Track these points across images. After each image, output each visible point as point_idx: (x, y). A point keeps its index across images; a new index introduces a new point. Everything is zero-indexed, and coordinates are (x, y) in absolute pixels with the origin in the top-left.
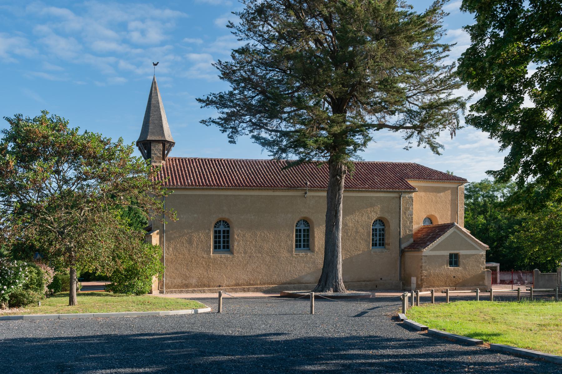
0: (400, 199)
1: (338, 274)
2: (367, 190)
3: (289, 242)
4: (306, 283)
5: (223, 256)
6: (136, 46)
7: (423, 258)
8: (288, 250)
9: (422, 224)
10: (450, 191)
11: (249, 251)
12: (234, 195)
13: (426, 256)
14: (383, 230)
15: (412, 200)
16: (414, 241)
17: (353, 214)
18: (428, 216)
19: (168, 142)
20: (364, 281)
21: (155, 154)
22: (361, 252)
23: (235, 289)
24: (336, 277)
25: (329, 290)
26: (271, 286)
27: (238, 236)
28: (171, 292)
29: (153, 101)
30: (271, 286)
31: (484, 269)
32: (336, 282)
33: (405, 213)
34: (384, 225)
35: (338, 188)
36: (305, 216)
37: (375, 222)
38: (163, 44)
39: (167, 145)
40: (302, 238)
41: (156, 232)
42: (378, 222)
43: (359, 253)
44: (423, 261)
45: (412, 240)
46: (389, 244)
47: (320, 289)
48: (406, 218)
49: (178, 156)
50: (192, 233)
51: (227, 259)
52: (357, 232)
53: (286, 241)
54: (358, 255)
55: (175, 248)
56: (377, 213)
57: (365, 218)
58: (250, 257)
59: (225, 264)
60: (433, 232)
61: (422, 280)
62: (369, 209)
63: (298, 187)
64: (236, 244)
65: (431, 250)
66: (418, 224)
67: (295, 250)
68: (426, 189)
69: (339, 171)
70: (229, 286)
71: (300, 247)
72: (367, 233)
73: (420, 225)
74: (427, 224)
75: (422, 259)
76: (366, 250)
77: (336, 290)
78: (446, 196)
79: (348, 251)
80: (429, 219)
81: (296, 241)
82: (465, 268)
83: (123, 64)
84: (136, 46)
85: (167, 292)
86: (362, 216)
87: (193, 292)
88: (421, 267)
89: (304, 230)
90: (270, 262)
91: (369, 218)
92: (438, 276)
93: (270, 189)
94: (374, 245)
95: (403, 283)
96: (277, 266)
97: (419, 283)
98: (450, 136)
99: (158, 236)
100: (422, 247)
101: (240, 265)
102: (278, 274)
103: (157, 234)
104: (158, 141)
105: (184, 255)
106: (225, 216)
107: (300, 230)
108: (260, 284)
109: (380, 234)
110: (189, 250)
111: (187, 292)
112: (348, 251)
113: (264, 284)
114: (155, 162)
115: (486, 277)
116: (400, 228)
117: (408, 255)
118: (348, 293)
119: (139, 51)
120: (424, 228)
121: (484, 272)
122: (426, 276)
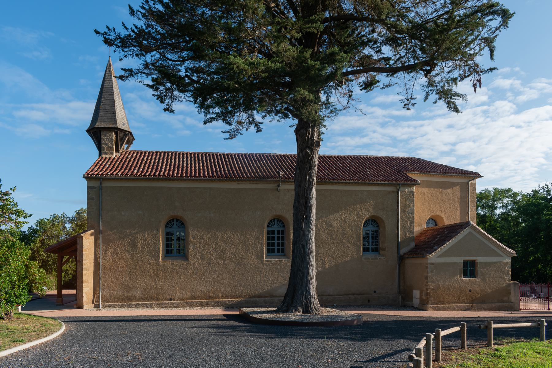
0: (398, 194)
1: (309, 287)
2: (356, 181)
3: (259, 246)
5: (175, 262)
7: (429, 266)
8: (257, 256)
9: (425, 226)
10: (458, 187)
11: (208, 256)
12: (189, 188)
13: (433, 264)
14: (377, 232)
15: (413, 195)
16: (416, 246)
17: (338, 212)
18: (432, 216)
19: (122, 130)
20: (353, 294)
21: (106, 144)
22: (349, 259)
23: (190, 303)
24: (307, 291)
25: (296, 310)
26: (236, 300)
27: (194, 238)
28: (110, 307)
29: (106, 85)
30: (236, 300)
31: (509, 281)
32: (306, 298)
34: (378, 226)
35: (308, 166)
36: (278, 214)
37: (366, 222)
39: (124, 136)
41: (89, 232)
42: (370, 222)
43: (347, 259)
44: (429, 270)
45: (413, 245)
46: (384, 249)
47: (285, 308)
48: (406, 216)
49: (137, 149)
50: (136, 233)
51: (180, 266)
53: (255, 245)
54: (346, 262)
56: (368, 211)
58: (209, 264)
59: (177, 272)
60: (440, 234)
61: (427, 294)
62: (359, 206)
63: (269, 178)
64: (191, 247)
65: (441, 256)
66: (420, 225)
67: (267, 256)
68: (429, 185)
69: (310, 142)
70: (182, 300)
71: (273, 252)
73: (423, 227)
74: (431, 225)
75: (427, 268)
76: (355, 256)
77: (306, 310)
78: (454, 193)
79: (333, 257)
80: (434, 220)
81: (268, 245)
82: (484, 280)
85: (104, 307)
86: (350, 214)
87: (137, 306)
88: (427, 278)
89: (278, 231)
90: (234, 270)
91: (358, 217)
92: (448, 289)
93: (234, 180)
94: (366, 250)
95: (402, 297)
97: (424, 298)
98: (473, 89)
99: (93, 237)
100: (427, 252)
101: (196, 274)
103: (91, 235)
104: (109, 129)
106: (179, 213)
107: (273, 231)
108: (223, 297)
109: (374, 236)
110: (133, 256)
111: (130, 306)
112: (333, 257)
113: (227, 297)
114: (106, 153)
115: (512, 291)
116: (398, 229)
117: (410, 262)
118: (326, 312)
120: (427, 230)
121: (509, 285)
122: (433, 289)
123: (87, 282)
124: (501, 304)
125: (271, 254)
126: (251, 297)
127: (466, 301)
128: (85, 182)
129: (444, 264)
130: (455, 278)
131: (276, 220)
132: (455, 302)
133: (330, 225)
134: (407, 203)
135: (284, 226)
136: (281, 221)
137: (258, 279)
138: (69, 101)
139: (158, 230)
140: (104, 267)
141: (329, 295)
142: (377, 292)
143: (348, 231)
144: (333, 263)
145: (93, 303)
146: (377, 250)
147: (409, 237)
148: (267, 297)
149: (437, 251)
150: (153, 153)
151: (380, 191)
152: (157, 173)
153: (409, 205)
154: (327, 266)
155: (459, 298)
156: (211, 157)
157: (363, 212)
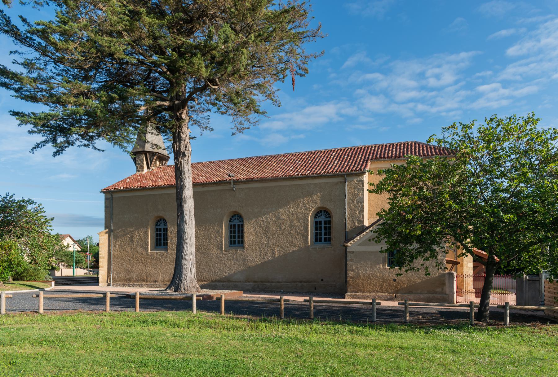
0: (345, 182)
3: (219, 239)
4: (236, 282)
6: (432, 89)
8: (218, 247)
12: (168, 194)
13: (353, 252)
17: (286, 206)
20: (301, 282)
27: (171, 233)
28: (117, 285)
33: (353, 201)
38: (456, 82)
40: (237, 234)
48: (355, 206)
50: (133, 231)
52: (292, 226)
54: (294, 252)
55: (120, 246)
56: (316, 203)
57: (301, 209)
62: (306, 199)
65: (360, 245)
70: (163, 282)
72: (304, 226)
79: (282, 247)
83: (420, 107)
84: (432, 89)
85: (113, 285)
86: (298, 207)
89: (325, 222)
91: (306, 209)
92: (369, 277)
96: (207, 263)
99: (107, 235)
102: (208, 271)
105: (127, 252)
106: (161, 214)
107: (235, 225)
111: (129, 286)
112: (282, 247)
119: (433, 93)
122: (352, 278)
123: (102, 267)
124: (431, 295)
125: (233, 245)
126: (213, 282)
127: (389, 290)
128: (103, 195)
129: (364, 252)
130: (377, 266)
131: (323, 212)
132: (377, 292)
133: (279, 218)
134: (356, 192)
135: (330, 217)
136: (327, 212)
137: (219, 266)
138: (304, 107)
139: (147, 228)
140: (114, 256)
141: (278, 282)
142: (324, 280)
143: (296, 223)
144: (282, 253)
145: (107, 282)
146: (328, 239)
147: (358, 226)
148: (225, 282)
149: (355, 240)
150: (390, 146)
151: (327, 183)
152: (363, 168)
153: (358, 194)
154: (277, 256)
155: (381, 288)
156: (417, 146)
157: (310, 204)
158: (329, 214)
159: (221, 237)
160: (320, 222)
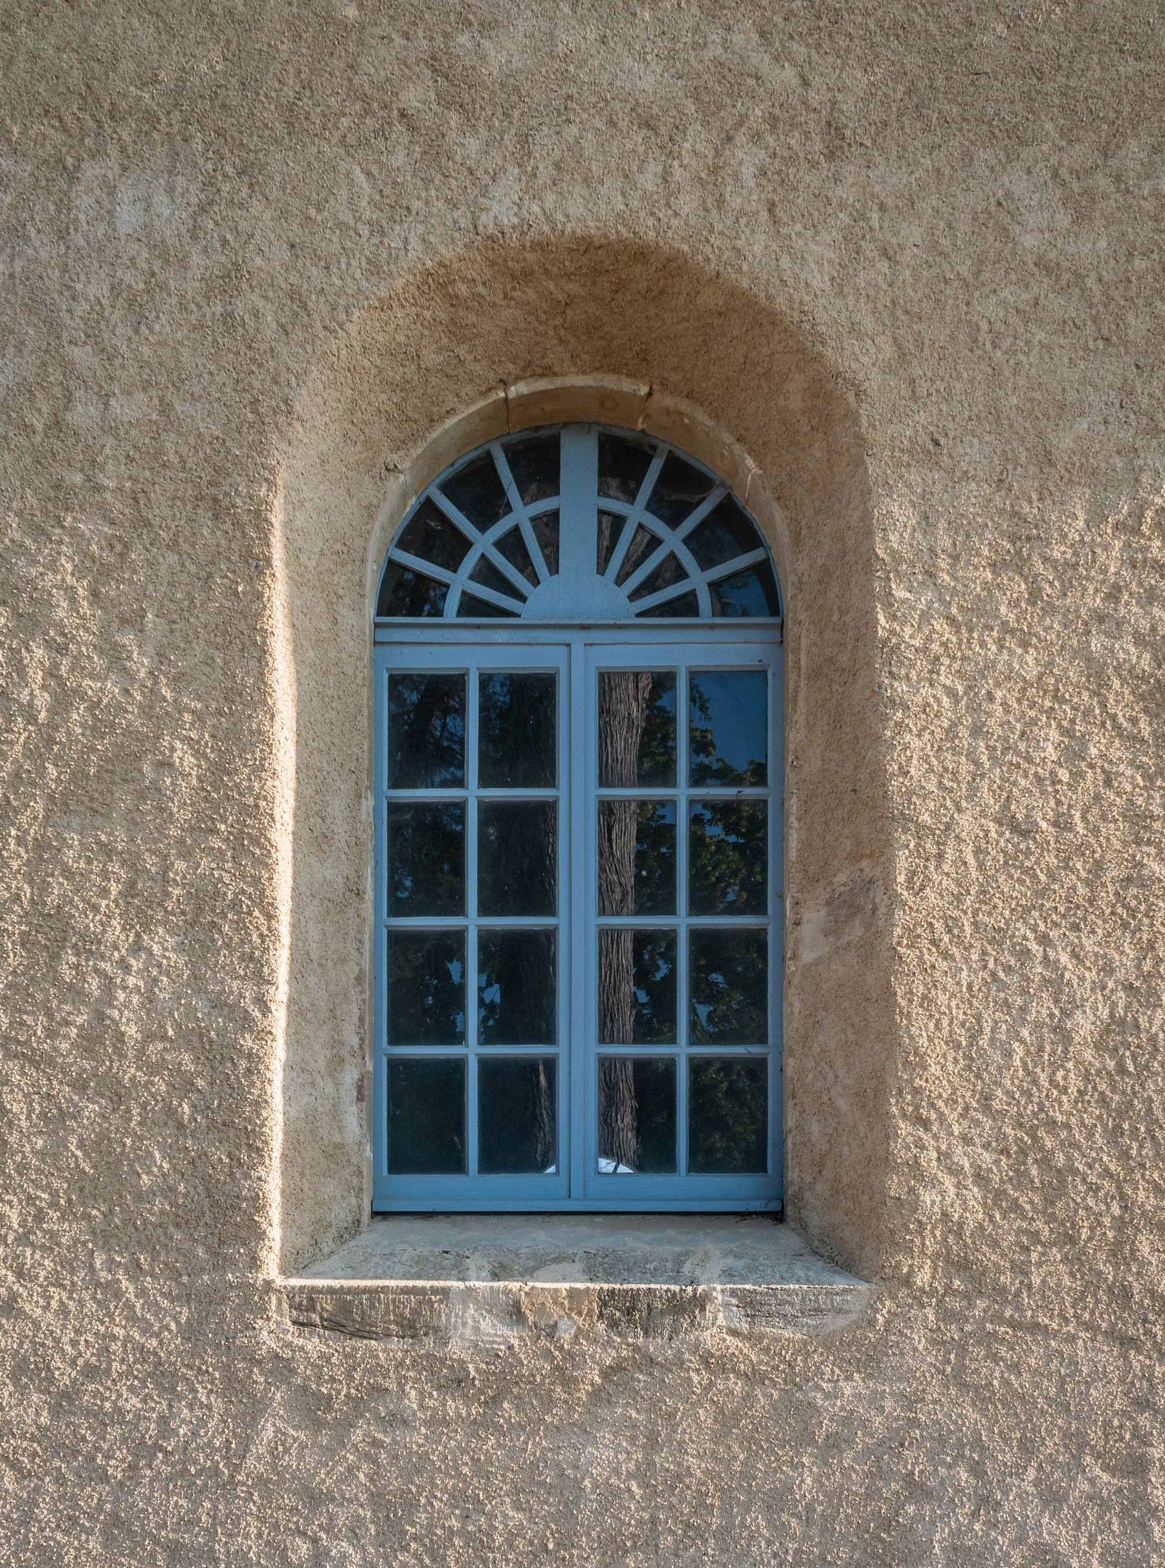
8: (104, 1183)
125: (474, 1185)
131: (579, 461)
135: (757, 593)
158: (732, 528)
159: (216, 923)
160: (523, 717)
